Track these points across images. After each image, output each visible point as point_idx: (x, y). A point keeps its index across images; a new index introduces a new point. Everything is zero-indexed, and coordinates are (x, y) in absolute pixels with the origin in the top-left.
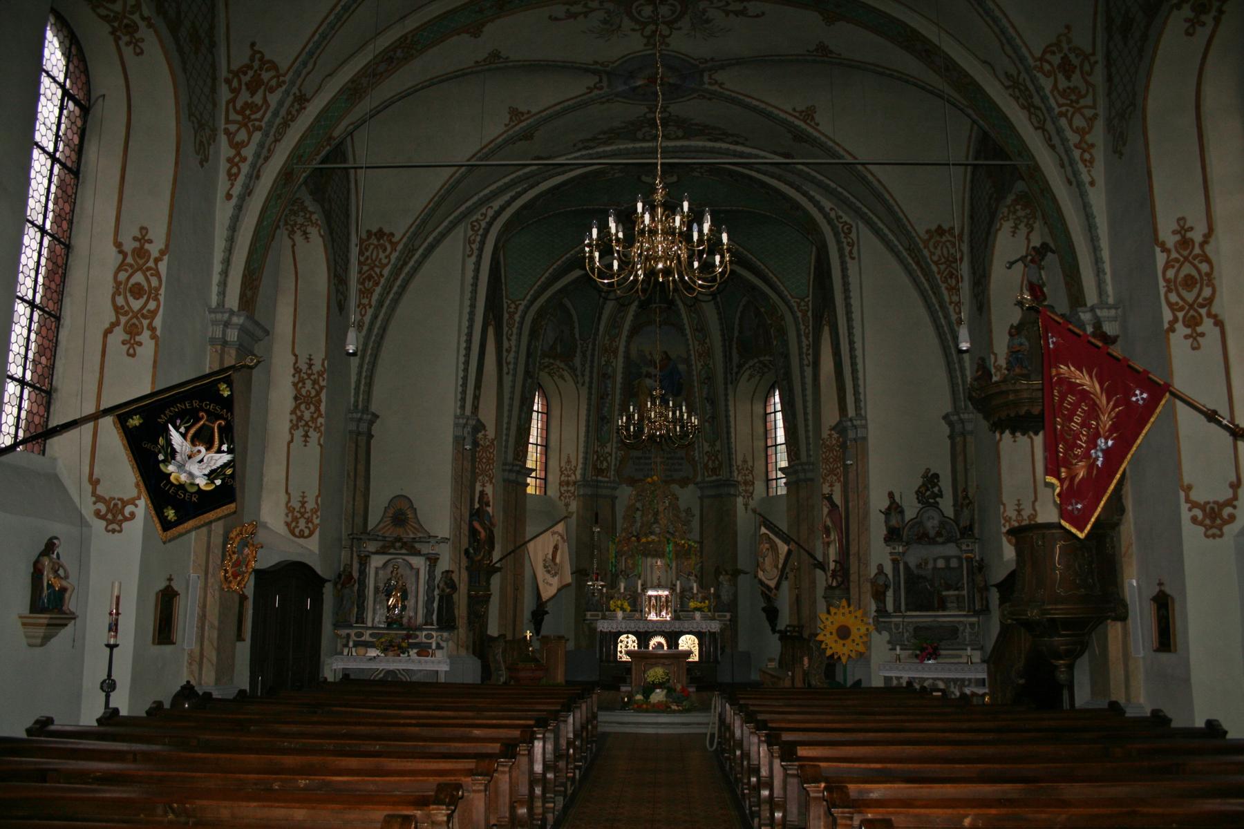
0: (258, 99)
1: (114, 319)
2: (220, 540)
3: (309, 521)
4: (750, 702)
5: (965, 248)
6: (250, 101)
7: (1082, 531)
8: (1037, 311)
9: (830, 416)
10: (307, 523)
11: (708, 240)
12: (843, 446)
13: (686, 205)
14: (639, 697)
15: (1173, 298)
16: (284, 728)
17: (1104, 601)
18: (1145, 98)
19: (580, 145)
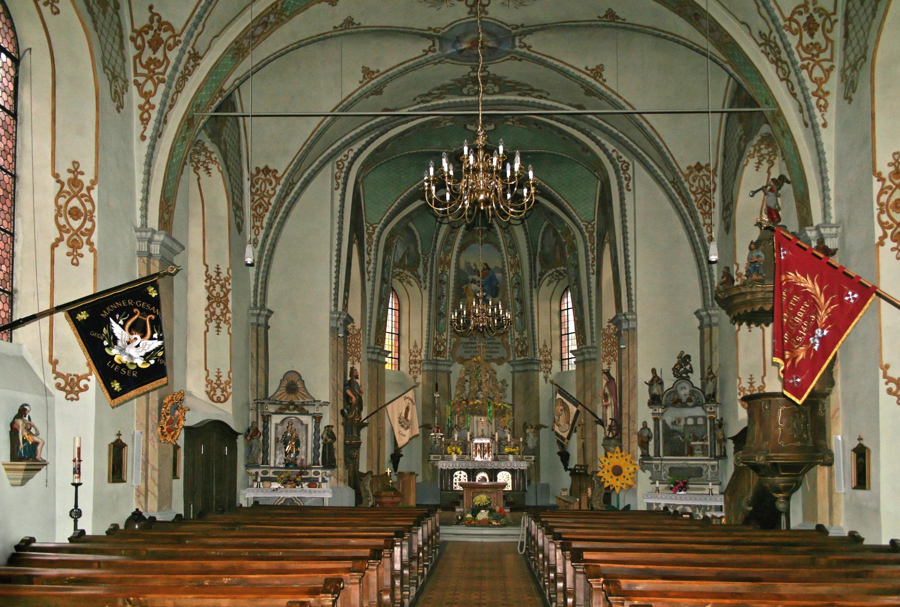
0: (159, 55)
1: (58, 236)
2: (156, 405)
3: (223, 390)
4: (549, 520)
5: (718, 180)
6: (153, 57)
7: (800, 398)
8: (772, 230)
9: (609, 311)
10: (222, 391)
11: (519, 176)
12: (619, 334)
13: (501, 148)
14: (469, 516)
15: (885, 218)
16: (211, 541)
17: (816, 452)
18: (875, 51)
19: (419, 100)
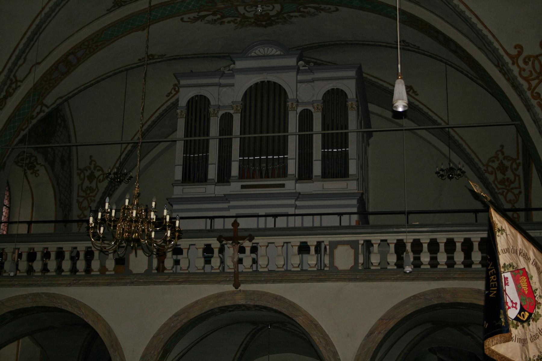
0: (94, 185)
